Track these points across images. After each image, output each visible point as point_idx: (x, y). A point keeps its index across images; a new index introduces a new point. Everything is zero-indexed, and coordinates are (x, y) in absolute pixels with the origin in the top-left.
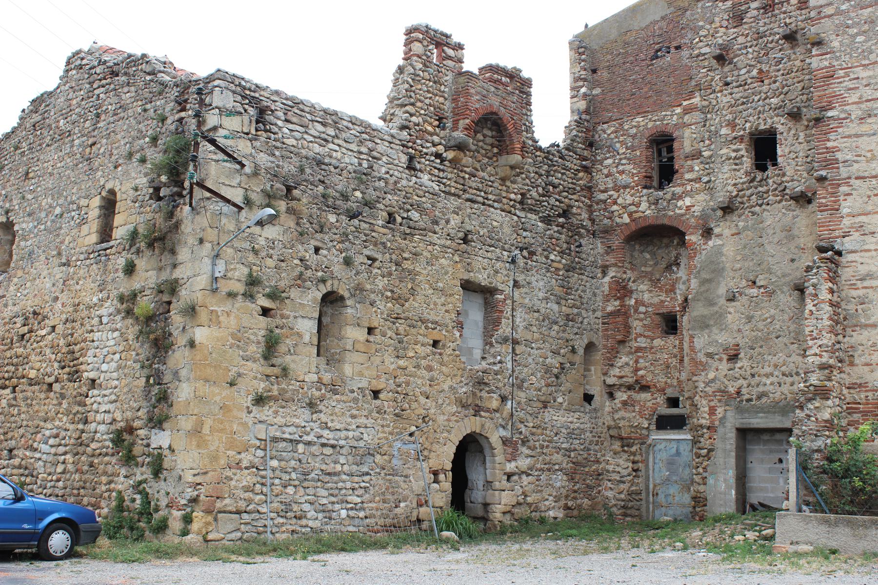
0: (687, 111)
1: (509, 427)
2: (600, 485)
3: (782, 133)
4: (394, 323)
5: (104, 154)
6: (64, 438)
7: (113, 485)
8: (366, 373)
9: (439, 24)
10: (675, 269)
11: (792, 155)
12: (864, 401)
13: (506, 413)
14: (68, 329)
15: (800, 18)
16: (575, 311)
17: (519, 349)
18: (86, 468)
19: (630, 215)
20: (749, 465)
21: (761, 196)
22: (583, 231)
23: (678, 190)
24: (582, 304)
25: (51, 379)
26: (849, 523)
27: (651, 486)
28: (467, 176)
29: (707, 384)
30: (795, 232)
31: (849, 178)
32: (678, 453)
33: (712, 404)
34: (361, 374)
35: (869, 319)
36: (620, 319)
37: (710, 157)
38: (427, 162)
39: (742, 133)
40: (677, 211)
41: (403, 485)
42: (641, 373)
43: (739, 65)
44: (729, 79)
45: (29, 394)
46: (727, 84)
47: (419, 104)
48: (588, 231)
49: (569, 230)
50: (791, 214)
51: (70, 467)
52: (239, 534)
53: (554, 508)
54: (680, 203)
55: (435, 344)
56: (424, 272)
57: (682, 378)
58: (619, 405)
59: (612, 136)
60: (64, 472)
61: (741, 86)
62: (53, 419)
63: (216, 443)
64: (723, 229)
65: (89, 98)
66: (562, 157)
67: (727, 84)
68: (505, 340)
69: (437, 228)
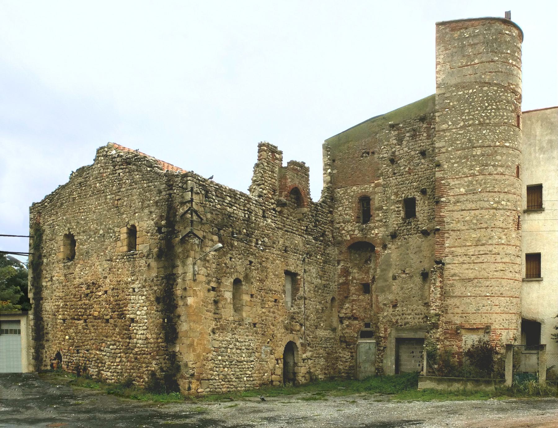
0: (377, 185)
1: (303, 338)
2: (337, 363)
3: (418, 201)
4: (260, 292)
5: (126, 206)
6: (119, 346)
7: (149, 368)
8: (251, 315)
9: (272, 142)
10: (369, 262)
11: (422, 212)
12: (450, 329)
13: (302, 332)
14: (115, 293)
15: (427, 144)
16: (328, 282)
17: (307, 301)
18: (133, 360)
19: (350, 236)
20: (400, 354)
21: (408, 230)
22: (330, 243)
24: (330, 279)
25: (108, 317)
27: (358, 364)
28: (285, 219)
31: (449, 230)
32: (370, 349)
33: (385, 327)
34: (249, 317)
35: (454, 294)
36: (345, 286)
37: (386, 210)
38: (270, 213)
39: (400, 199)
40: (372, 235)
41: (266, 365)
42: (354, 311)
43: (401, 164)
44: (396, 171)
45: (95, 324)
46: (395, 174)
47: (266, 184)
48: (332, 243)
49: (324, 243)
51: (124, 359)
52: (209, 389)
53: (320, 374)
54: (373, 232)
55: (276, 301)
56: (271, 267)
58: (345, 327)
59: (342, 195)
60: (120, 362)
61: (401, 175)
62: (112, 336)
63: (199, 350)
65: (114, 174)
66: (321, 207)
67: (395, 174)
68: (301, 298)
69: (275, 246)
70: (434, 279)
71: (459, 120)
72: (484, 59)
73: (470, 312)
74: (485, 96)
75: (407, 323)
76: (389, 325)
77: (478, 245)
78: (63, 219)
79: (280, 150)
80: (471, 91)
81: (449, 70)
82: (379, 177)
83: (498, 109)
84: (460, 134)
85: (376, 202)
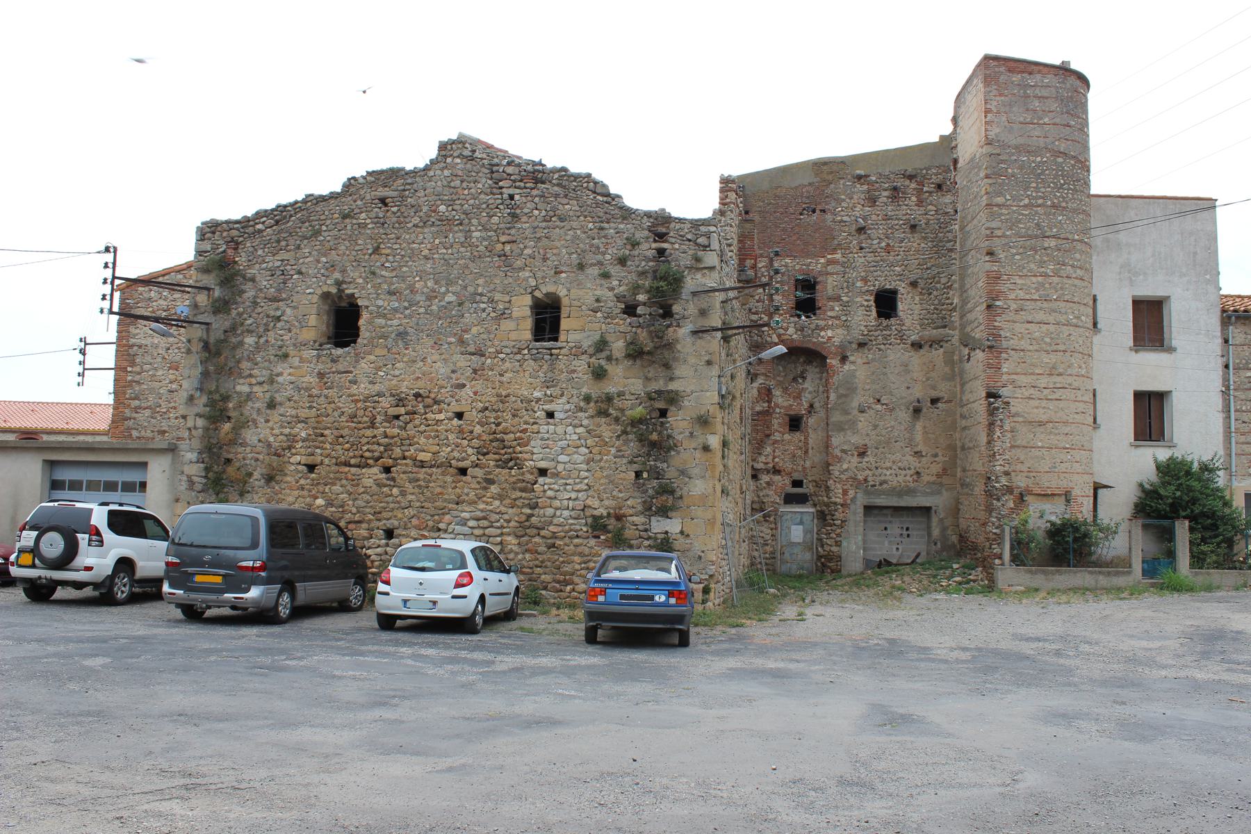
10: (800, 381)
23: (821, 323)
26: (1044, 572)
29: (842, 473)
30: (910, 367)
33: (845, 487)
37: (848, 302)
39: (872, 288)
42: (777, 460)
44: (863, 245)
46: (861, 248)
50: (907, 354)
54: (822, 333)
57: (806, 466)
64: (856, 357)
67: (861, 248)
70: (1001, 420)
71: (1022, 195)
72: (1057, 120)
73: (1042, 470)
74: (1060, 170)
75: (885, 482)
76: (851, 485)
77: (1053, 375)
78: (318, 261)
79: (551, 166)
80: (1039, 159)
81: (1006, 123)
82: (835, 249)
83: (1075, 191)
84: (1023, 214)
85: (829, 287)
